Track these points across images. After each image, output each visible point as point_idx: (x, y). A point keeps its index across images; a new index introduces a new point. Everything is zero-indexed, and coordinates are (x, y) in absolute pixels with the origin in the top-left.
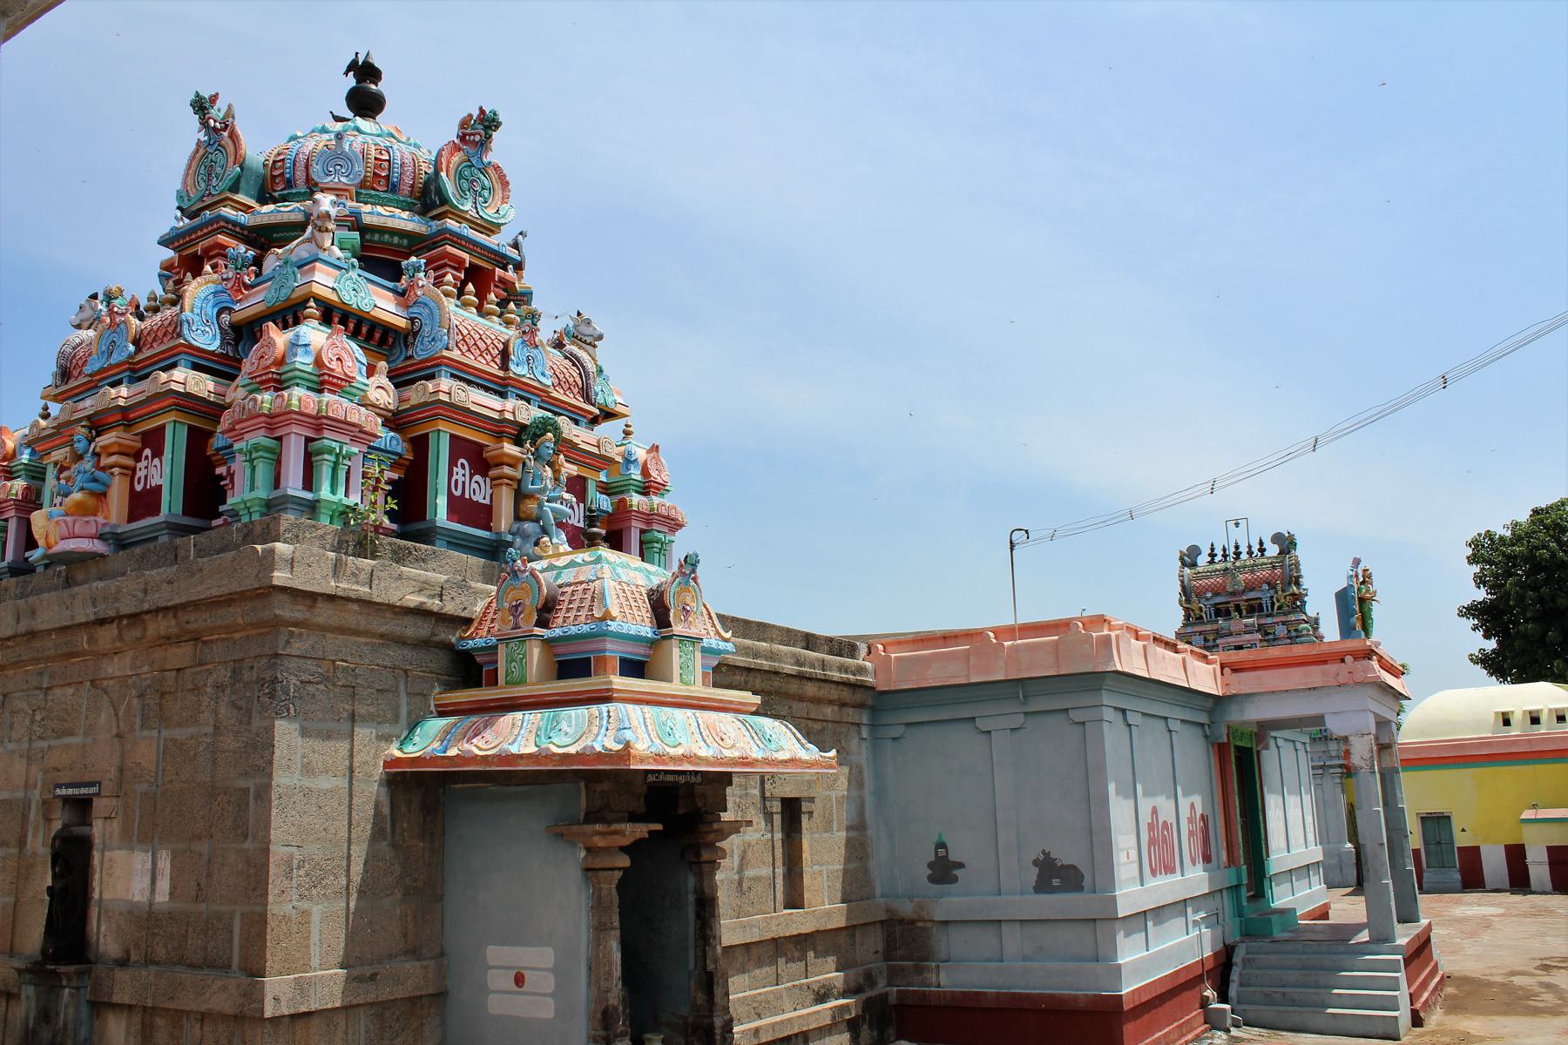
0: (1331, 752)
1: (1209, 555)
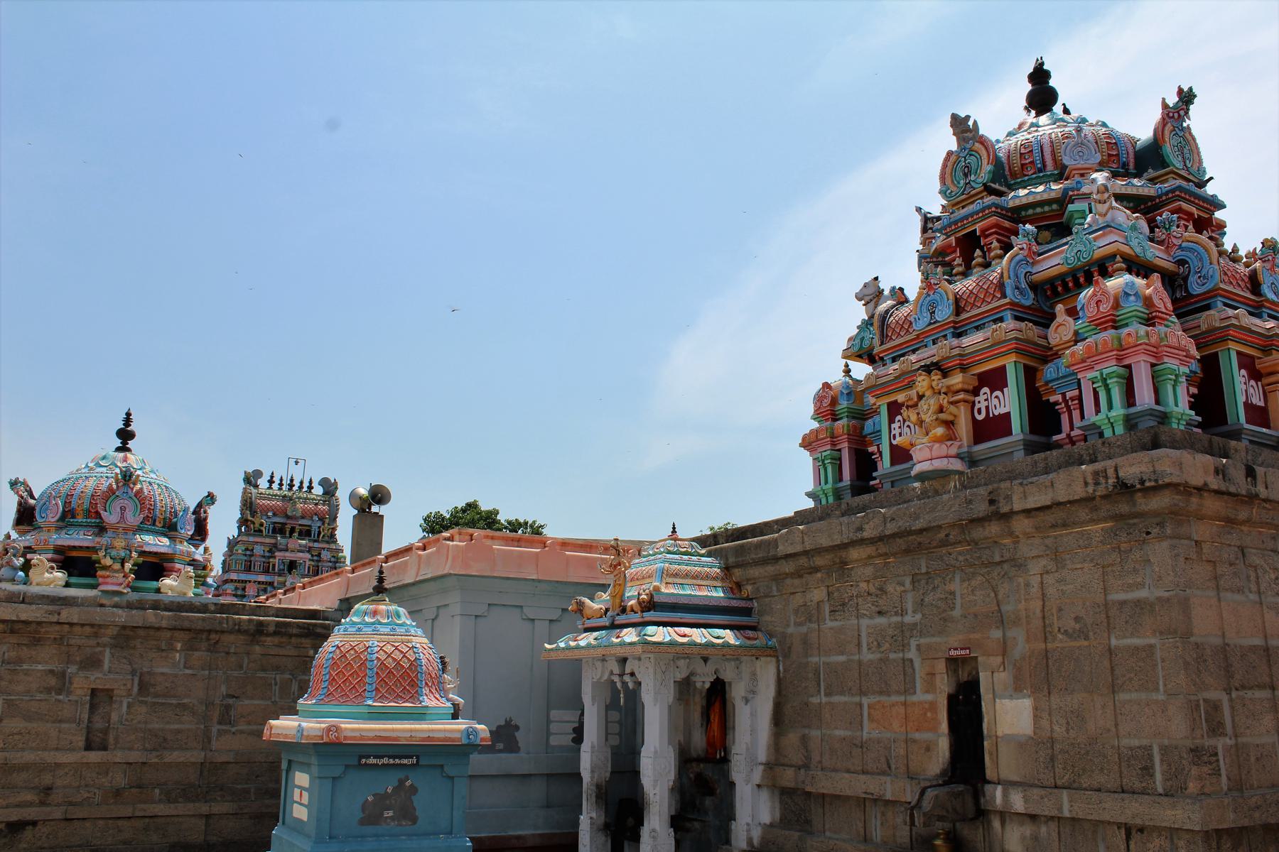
1: (269, 481)
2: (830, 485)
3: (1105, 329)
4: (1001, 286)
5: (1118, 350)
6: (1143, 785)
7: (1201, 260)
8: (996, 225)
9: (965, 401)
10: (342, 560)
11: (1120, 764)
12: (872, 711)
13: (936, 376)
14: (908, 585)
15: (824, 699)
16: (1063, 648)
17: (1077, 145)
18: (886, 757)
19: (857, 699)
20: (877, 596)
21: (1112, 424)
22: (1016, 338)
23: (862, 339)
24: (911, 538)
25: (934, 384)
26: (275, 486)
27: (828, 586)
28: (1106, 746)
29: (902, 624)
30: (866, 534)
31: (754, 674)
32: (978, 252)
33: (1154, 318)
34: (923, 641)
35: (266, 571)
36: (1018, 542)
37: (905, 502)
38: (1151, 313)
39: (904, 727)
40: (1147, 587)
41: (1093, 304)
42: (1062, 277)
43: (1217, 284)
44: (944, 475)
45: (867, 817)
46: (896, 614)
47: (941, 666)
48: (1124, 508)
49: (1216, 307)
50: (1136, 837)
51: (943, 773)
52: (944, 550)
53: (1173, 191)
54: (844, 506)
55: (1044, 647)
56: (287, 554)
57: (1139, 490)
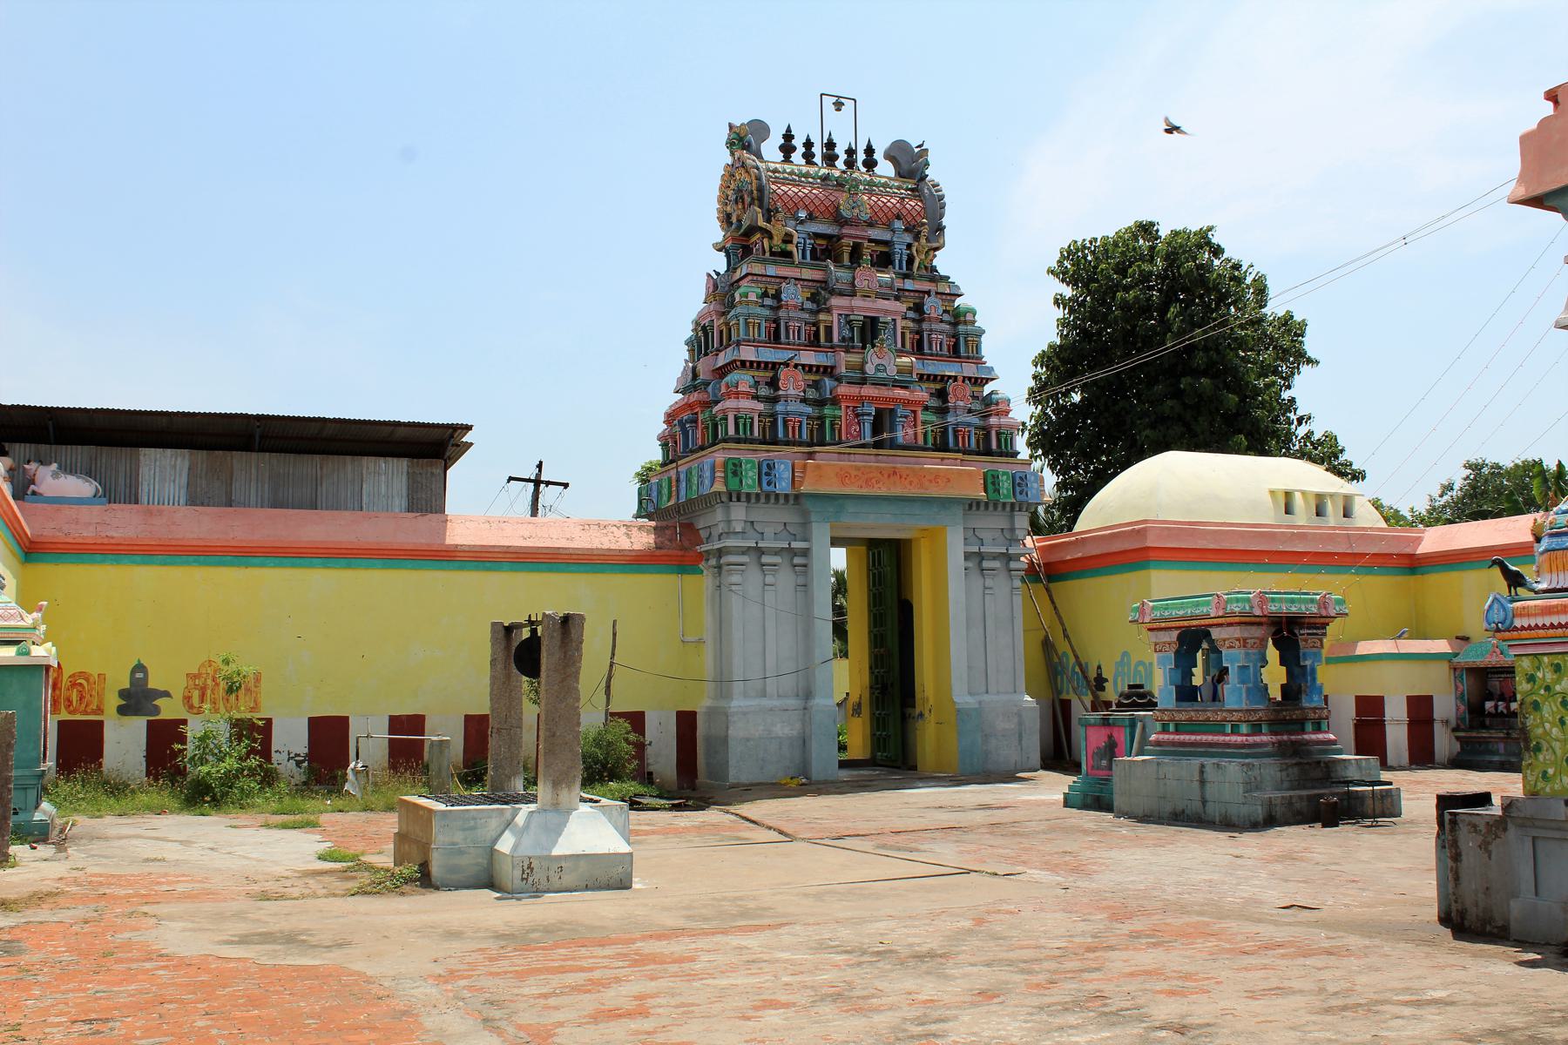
0: (734, 524)
10: (969, 317)
26: (797, 157)
35: (814, 343)
56: (857, 302)
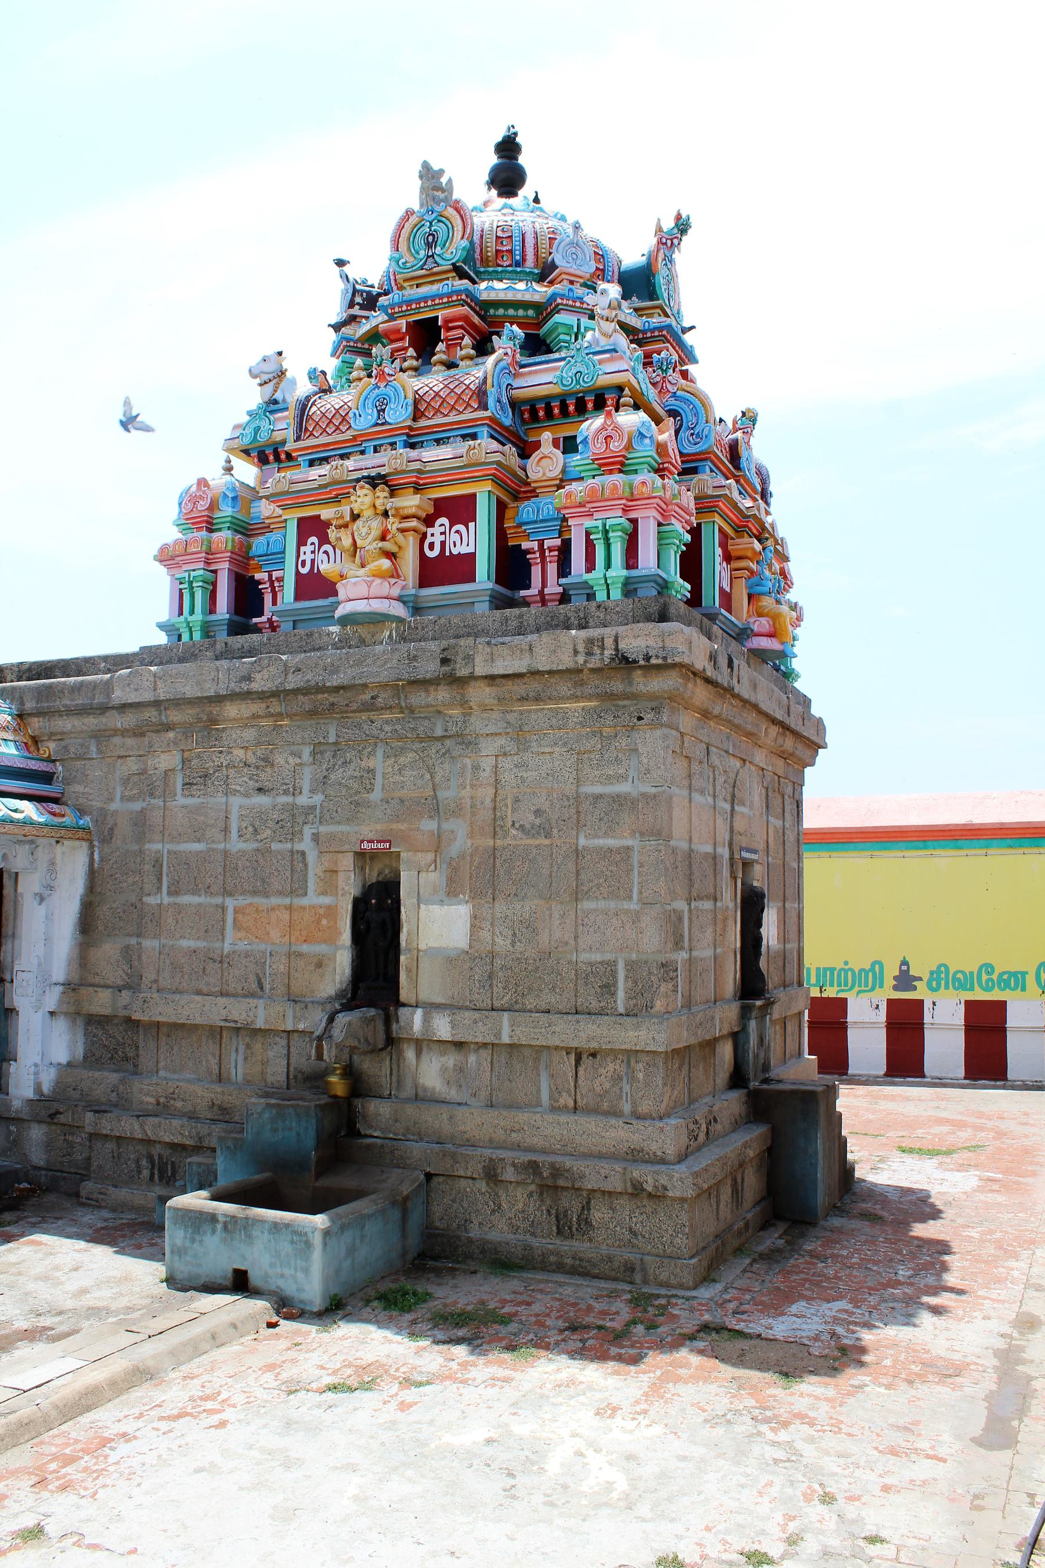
2: (198, 616)
3: (611, 472)
4: (481, 394)
5: (627, 500)
6: (601, 1004)
7: (696, 415)
8: (466, 319)
9: (415, 530)
11: (576, 981)
12: (240, 917)
13: (382, 492)
14: (306, 756)
15: (167, 900)
16: (516, 846)
17: (571, 243)
18: (257, 975)
19: (219, 900)
20: (257, 768)
21: (608, 585)
22: (498, 463)
23: (257, 430)
24: (320, 696)
25: (378, 503)
27: (183, 751)
28: (562, 961)
29: (294, 805)
30: (255, 686)
31: (52, 863)
32: (441, 347)
33: (664, 469)
34: (323, 829)
36: (470, 714)
37: (314, 650)
38: (663, 464)
39: (287, 937)
40: (630, 780)
41: (601, 438)
42: (547, 400)
43: (711, 447)
44: (377, 619)
45: (223, 1050)
46: (286, 792)
47: (347, 862)
48: (617, 686)
49: (705, 472)
50: (586, 1061)
51: (340, 995)
52: (364, 716)
53: (660, 329)
54: (219, 646)
55: (491, 843)
57: (640, 667)
